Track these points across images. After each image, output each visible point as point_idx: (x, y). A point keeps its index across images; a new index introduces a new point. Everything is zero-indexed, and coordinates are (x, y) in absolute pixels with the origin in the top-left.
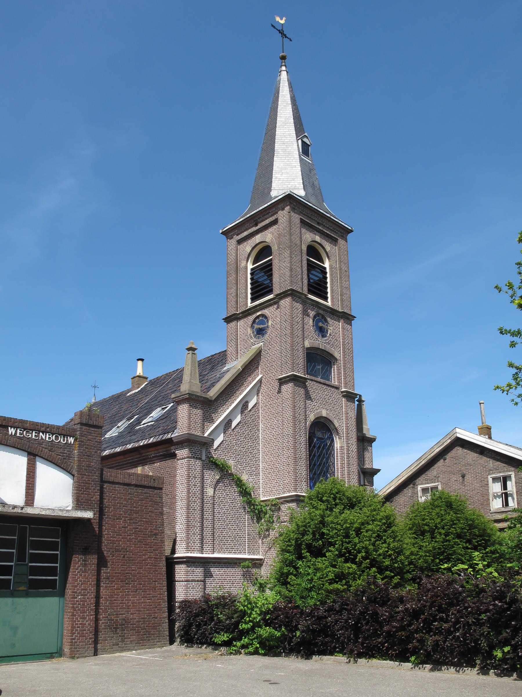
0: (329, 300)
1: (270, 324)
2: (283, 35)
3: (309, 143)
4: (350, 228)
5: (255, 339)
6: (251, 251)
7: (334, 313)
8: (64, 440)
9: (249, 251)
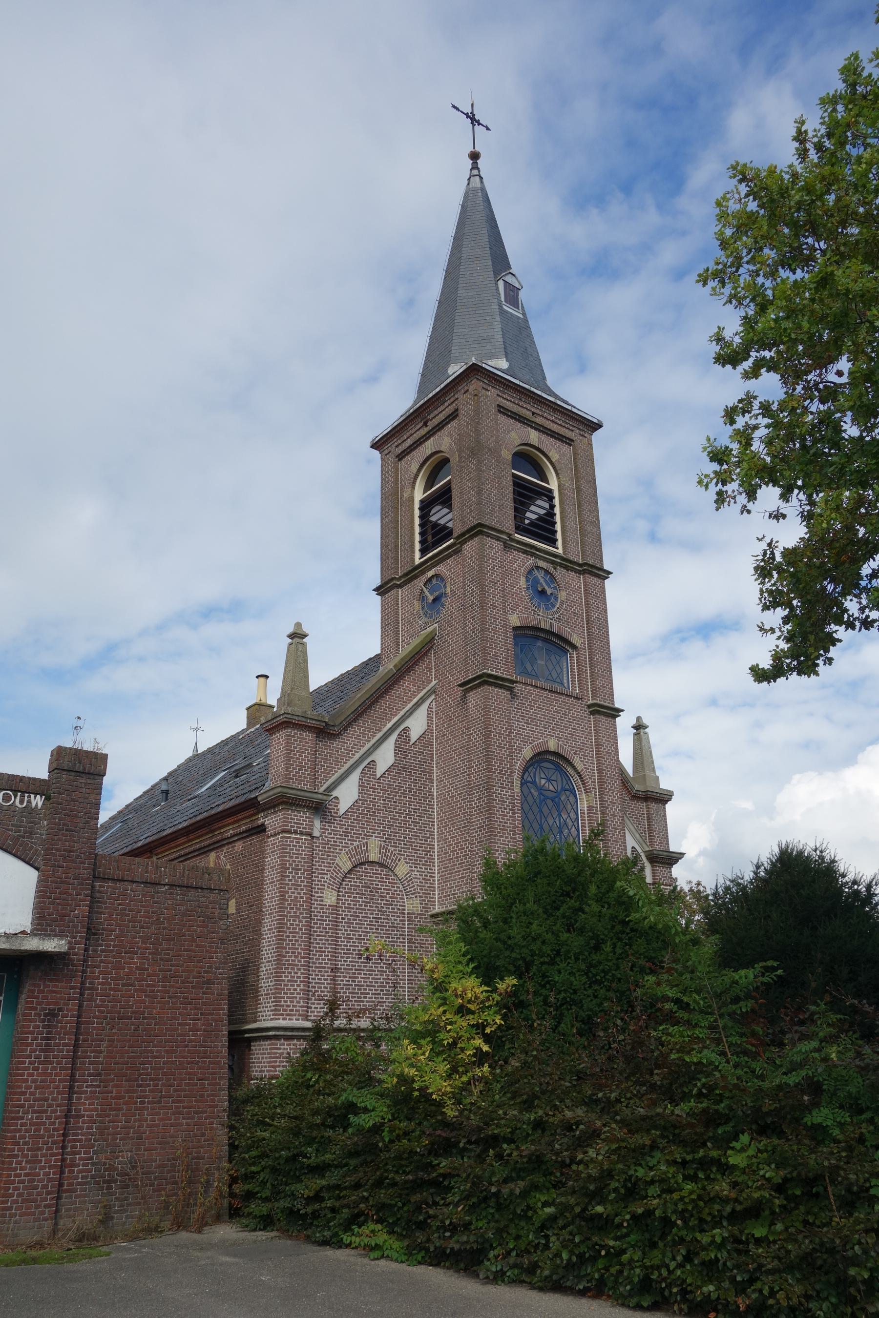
0: (560, 544)
1: (448, 590)
2: (473, 119)
3: (517, 285)
4: (596, 421)
5: (426, 620)
6: (419, 470)
7: (567, 564)
8: (22, 802)
9: (415, 471)
